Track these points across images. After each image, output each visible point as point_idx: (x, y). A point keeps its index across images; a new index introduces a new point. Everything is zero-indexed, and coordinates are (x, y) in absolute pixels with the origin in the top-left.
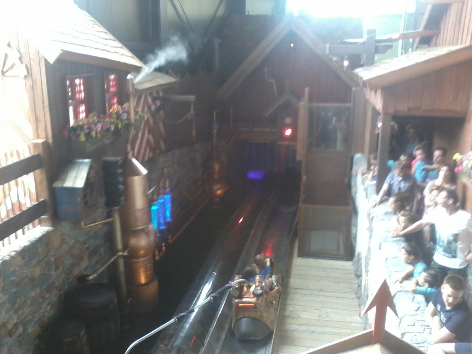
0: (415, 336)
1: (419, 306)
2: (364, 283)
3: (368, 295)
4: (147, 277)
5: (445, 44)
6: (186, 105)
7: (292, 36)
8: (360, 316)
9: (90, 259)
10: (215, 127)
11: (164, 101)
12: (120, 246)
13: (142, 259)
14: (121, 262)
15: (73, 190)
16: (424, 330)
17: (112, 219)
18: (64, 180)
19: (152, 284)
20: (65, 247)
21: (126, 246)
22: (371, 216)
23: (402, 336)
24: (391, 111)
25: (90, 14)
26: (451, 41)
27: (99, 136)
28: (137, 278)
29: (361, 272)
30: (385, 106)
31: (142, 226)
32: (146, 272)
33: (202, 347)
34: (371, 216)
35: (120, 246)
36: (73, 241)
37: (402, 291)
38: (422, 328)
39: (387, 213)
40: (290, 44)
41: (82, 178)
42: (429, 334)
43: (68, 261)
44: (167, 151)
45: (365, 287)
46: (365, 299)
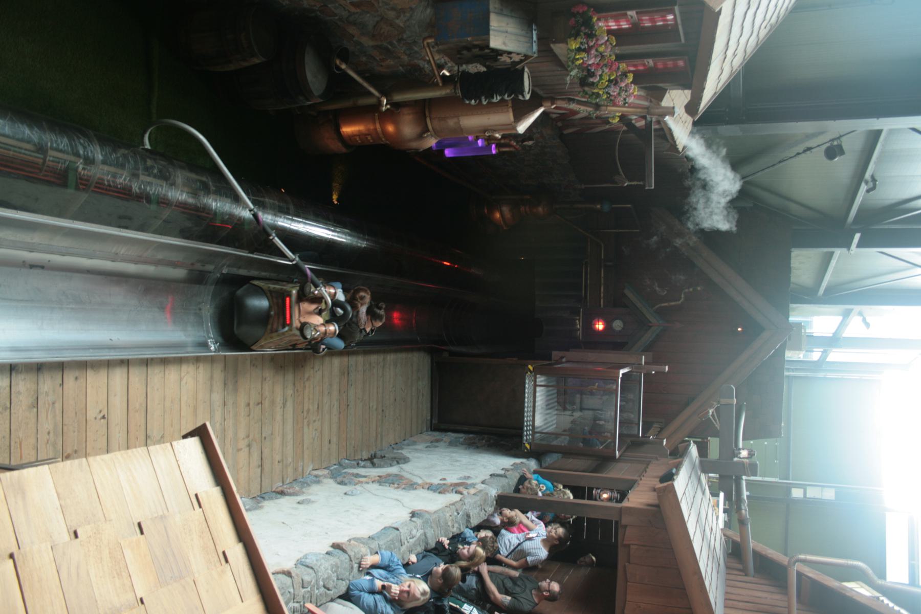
0: (285, 522)
1: (330, 589)
2: (363, 474)
3: (345, 484)
4: (352, 136)
5: (727, 586)
6: (638, 172)
7: (754, 330)
8: (313, 470)
9: (376, 47)
10: (606, 207)
11: (645, 133)
12: (399, 98)
13: (378, 126)
14: (371, 101)
15: (485, 30)
16: (297, 602)
17: (441, 84)
18: (500, 13)
19: (340, 144)
20: (391, 14)
21: (396, 106)
22: (461, 489)
23: (287, 573)
24: (625, 520)
25: (791, 12)
26: (733, 597)
27: (578, 63)
28: (351, 121)
29: (380, 466)
30: (630, 510)
31: (433, 128)
32: (360, 134)
33: (247, 252)
34: (461, 489)
35: (399, 98)
36: (401, 25)
37: (351, 562)
38: (300, 599)
39: (468, 516)
40: (742, 328)
41: (504, 44)
42: (292, 610)
43: (369, 20)
44: (562, 136)
45: (357, 475)
46: (339, 479)
